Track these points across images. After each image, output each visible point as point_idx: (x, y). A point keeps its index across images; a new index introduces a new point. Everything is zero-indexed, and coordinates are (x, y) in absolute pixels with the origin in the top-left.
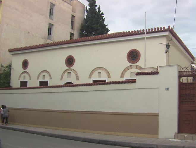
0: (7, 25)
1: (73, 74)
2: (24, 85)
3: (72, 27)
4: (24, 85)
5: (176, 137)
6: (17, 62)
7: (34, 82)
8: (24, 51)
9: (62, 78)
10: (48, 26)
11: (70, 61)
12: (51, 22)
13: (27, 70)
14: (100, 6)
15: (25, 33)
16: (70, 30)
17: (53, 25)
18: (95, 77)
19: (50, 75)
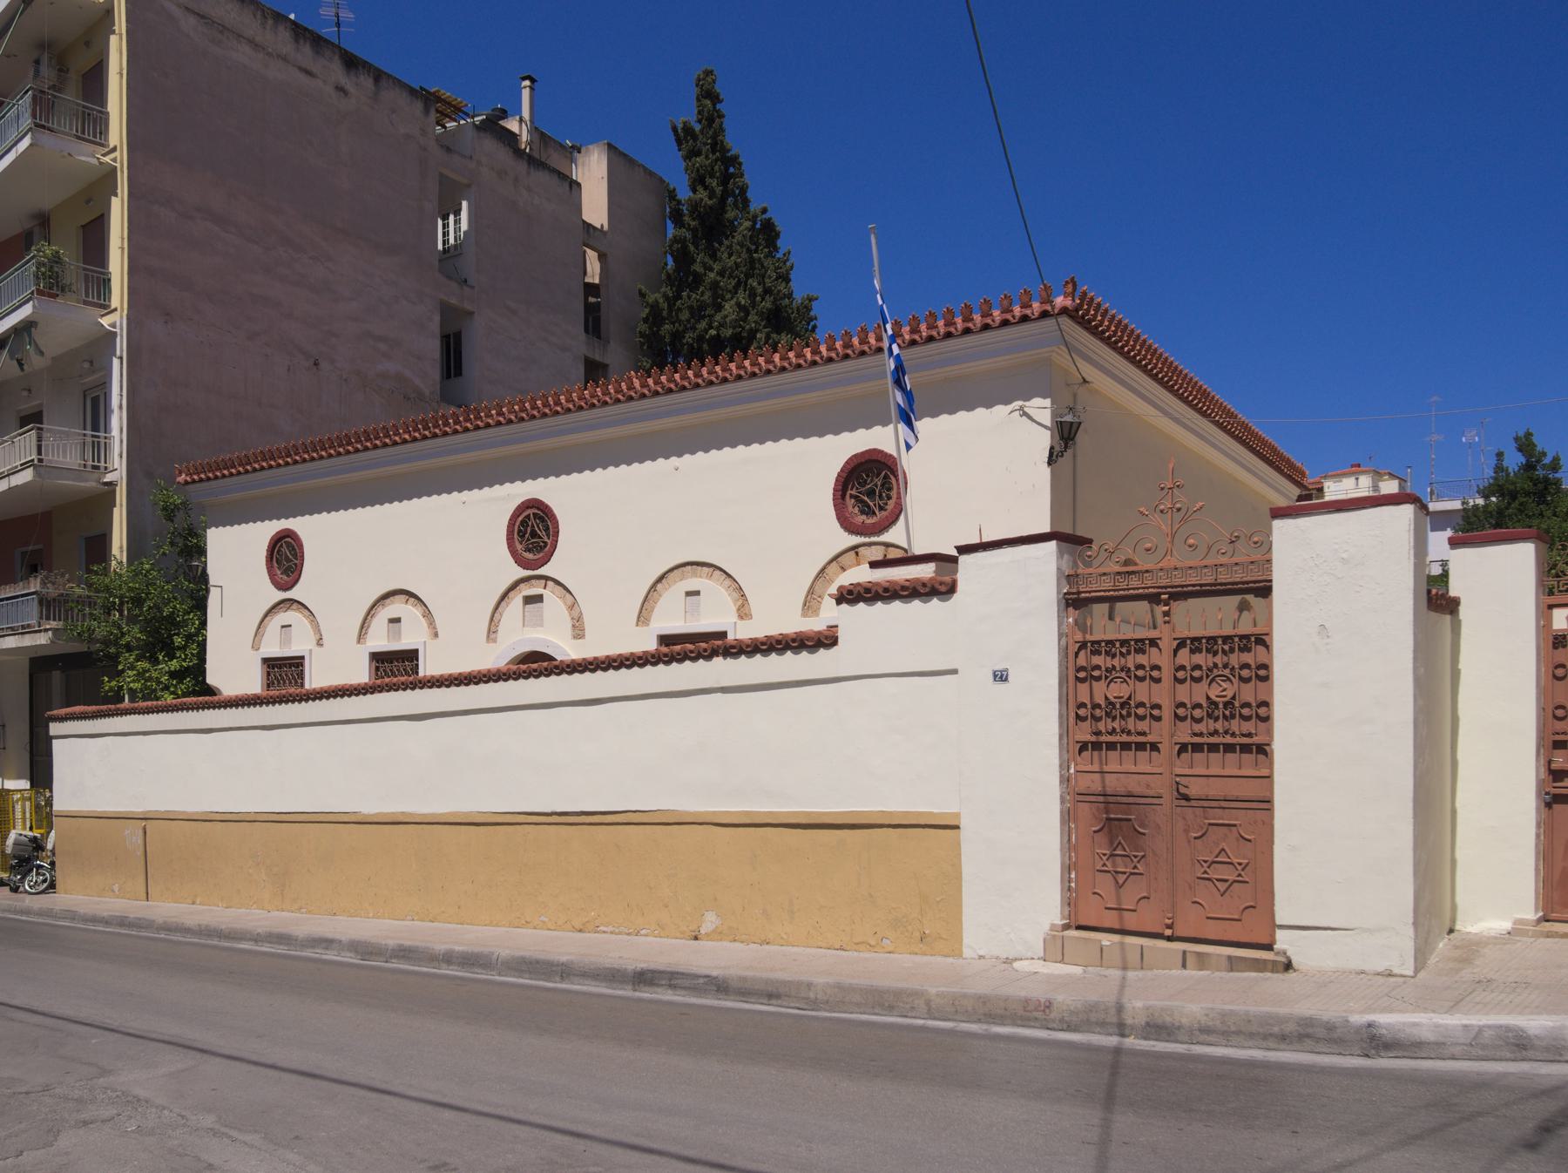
1: (553, 601)
2: (284, 677)
4: (284, 677)
5: (1055, 948)
7: (337, 660)
10: (437, 318)
11: (534, 534)
14: (708, 94)
17: (471, 313)
18: (673, 618)
19: (428, 614)
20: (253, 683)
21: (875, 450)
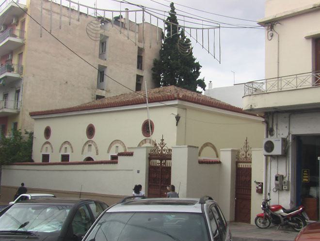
0: (34, 75)
1: (93, 147)
2: (46, 158)
3: (140, 66)
6: (38, 129)
7: (55, 158)
8: (43, 117)
9: (83, 151)
12: (103, 63)
13: (48, 140)
15: (60, 84)
16: (135, 72)
17: (106, 67)
20: (59, 160)
21: (88, 127)
